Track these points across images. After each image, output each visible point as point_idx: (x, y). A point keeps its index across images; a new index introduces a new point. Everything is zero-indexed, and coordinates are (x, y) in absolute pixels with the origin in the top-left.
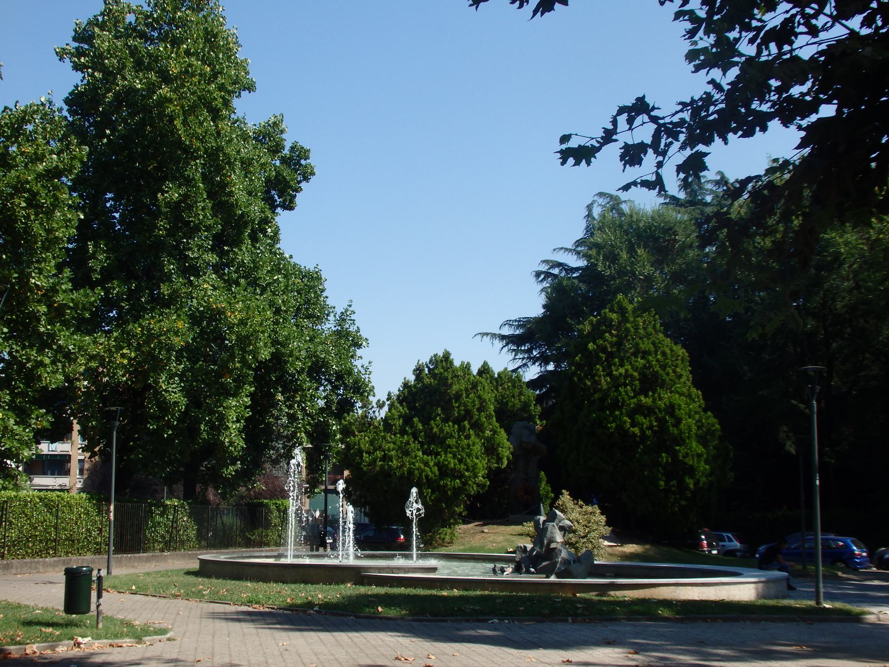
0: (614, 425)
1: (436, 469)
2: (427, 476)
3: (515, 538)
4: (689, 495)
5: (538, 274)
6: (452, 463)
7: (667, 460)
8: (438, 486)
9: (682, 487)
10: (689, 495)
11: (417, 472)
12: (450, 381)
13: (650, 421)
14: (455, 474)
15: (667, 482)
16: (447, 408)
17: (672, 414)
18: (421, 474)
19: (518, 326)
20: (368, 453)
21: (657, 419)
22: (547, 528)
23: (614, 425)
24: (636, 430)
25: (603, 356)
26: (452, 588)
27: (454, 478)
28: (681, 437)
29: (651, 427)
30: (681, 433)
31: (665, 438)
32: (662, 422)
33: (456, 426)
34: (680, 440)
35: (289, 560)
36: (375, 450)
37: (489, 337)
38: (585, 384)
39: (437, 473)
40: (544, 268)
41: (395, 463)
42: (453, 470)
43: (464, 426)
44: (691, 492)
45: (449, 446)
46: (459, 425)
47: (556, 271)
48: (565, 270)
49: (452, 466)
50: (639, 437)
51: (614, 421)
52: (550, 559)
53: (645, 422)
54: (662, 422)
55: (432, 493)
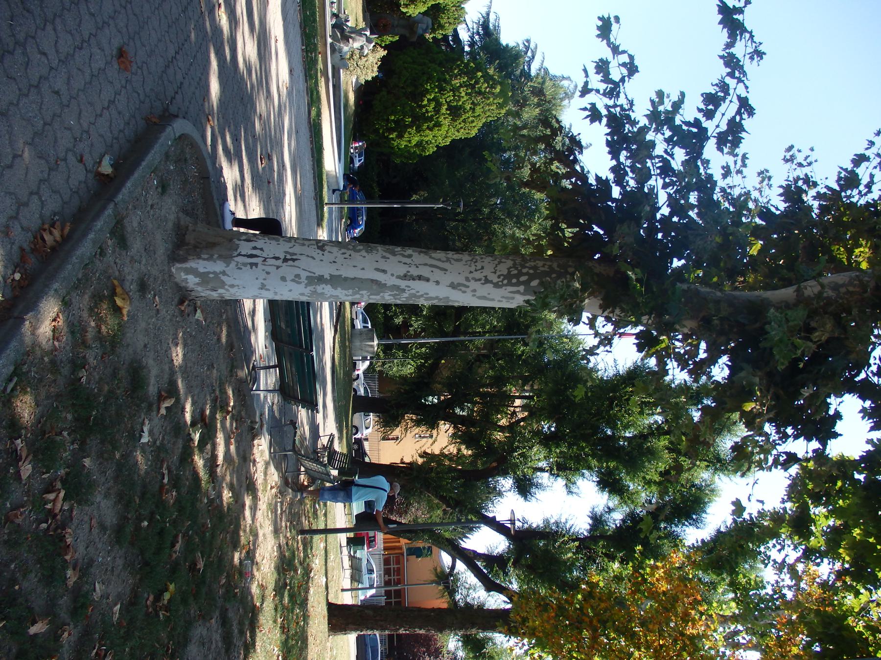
3: (354, 16)
5: (528, 41)
24: (425, 102)
25: (473, 82)
29: (427, 112)
32: (430, 119)
40: (532, 46)
47: (529, 54)
53: (430, 109)
54: (430, 119)
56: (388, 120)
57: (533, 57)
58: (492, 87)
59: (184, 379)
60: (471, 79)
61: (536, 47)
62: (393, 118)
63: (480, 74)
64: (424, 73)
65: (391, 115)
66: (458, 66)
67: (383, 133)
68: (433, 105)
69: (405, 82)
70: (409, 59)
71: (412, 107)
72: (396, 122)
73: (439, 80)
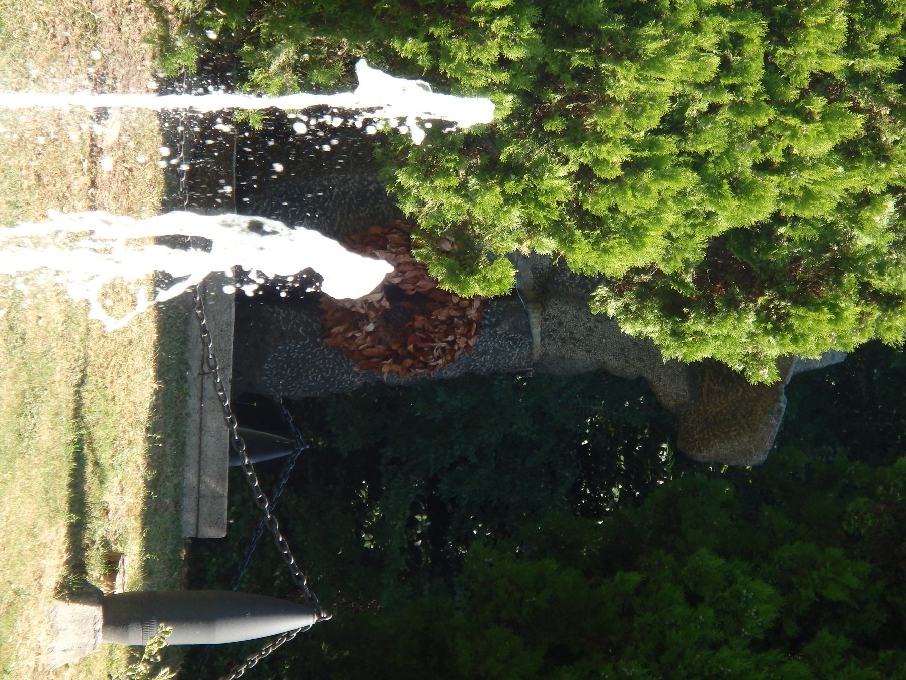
49: (624, 82)
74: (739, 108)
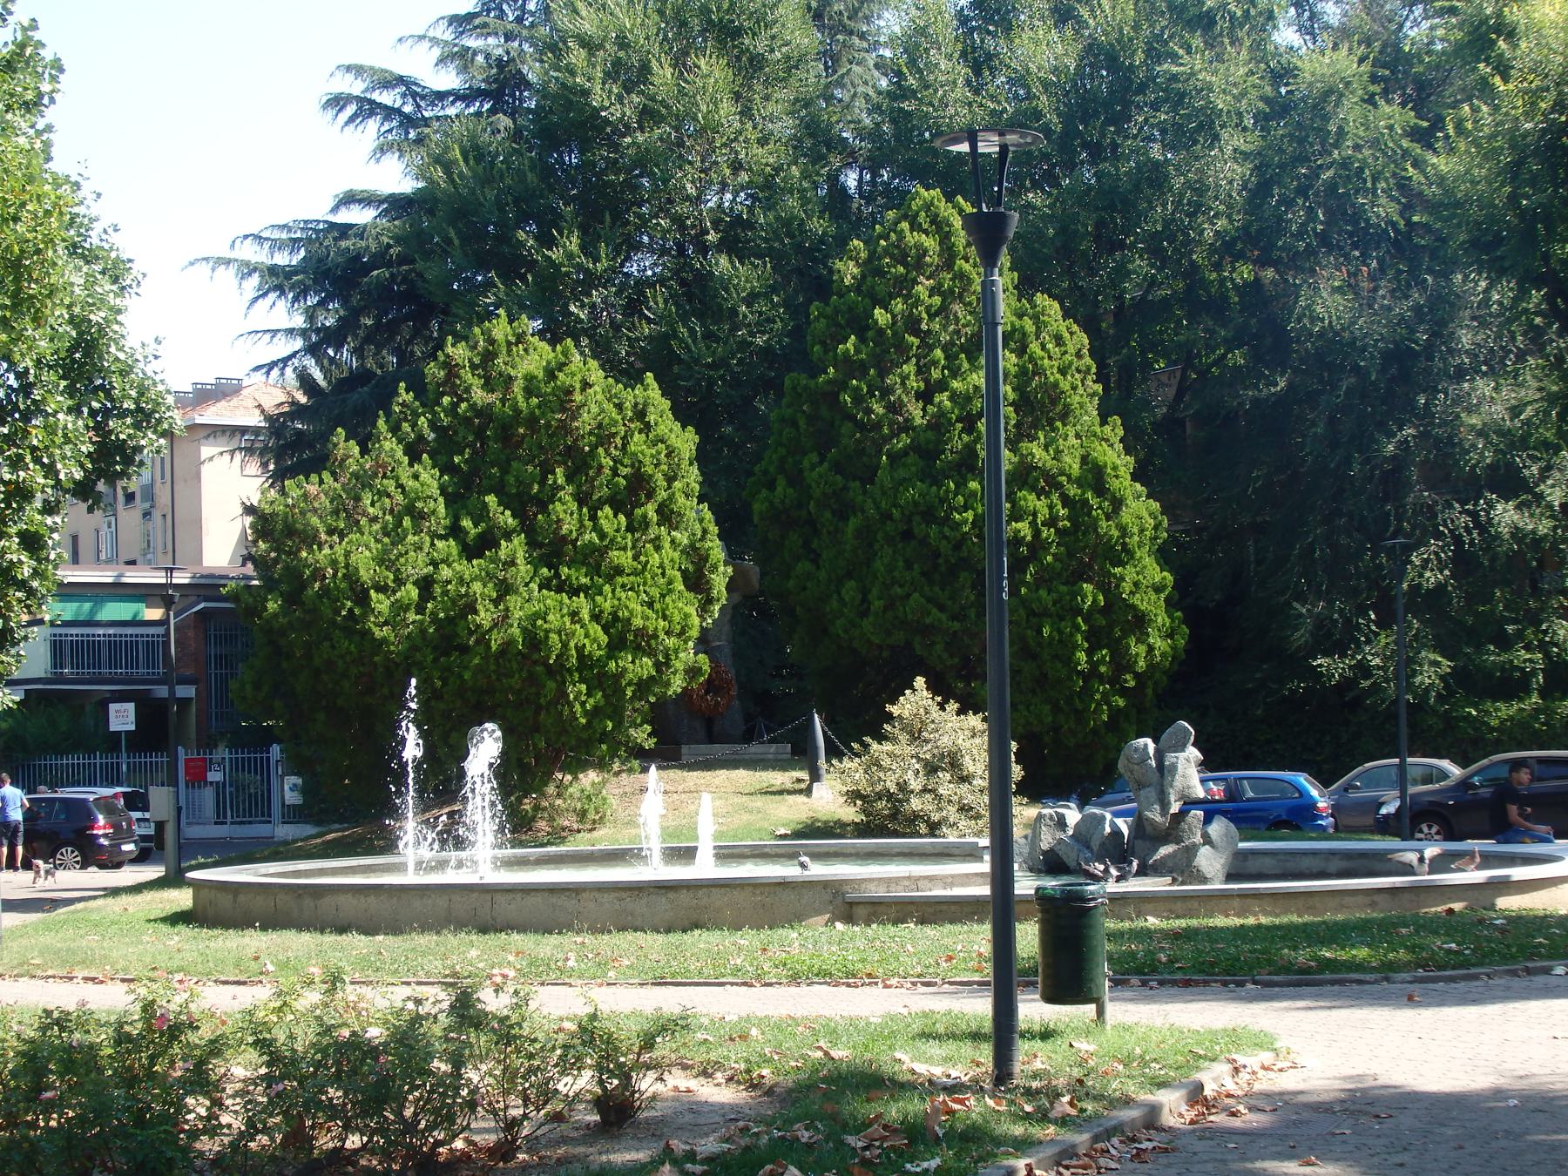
0: (970, 515)
1: (596, 630)
2: (580, 649)
3: (759, 802)
4: (1132, 684)
5: (337, 102)
6: (638, 614)
7: (1094, 601)
8: (603, 675)
9: (1122, 663)
10: (1132, 684)
11: (554, 637)
12: (578, 397)
13: (1051, 507)
14: (642, 643)
15: (1090, 653)
16: (580, 465)
17: (1101, 489)
18: (565, 645)
19: (277, 245)
20: (382, 589)
21: (1066, 501)
22: (1174, 767)
23: (970, 515)
24: (1024, 528)
25: (913, 340)
26: (1140, 914)
27: (638, 650)
28: (1124, 544)
29: (1052, 521)
30: (1123, 529)
31: (1088, 550)
32: (1077, 507)
33: (622, 518)
34: (1120, 554)
35: (411, 878)
36: (400, 582)
37: (232, 269)
38: (869, 411)
39: (604, 639)
40: (357, 87)
41: (484, 617)
42: (640, 632)
43: (645, 516)
44: (1137, 676)
45: (619, 571)
46: (629, 515)
47: (387, 98)
48: (414, 95)
49: (638, 622)
50: (1029, 545)
51: (966, 508)
52: (1178, 840)
53: (1040, 505)
54: (1077, 507)
55: (589, 695)
56: (1092, 674)
57: (401, 80)
58: (916, 262)
59: (24, 845)
60: (903, 349)
61: (357, 70)
62: (1082, 656)
63: (881, 316)
64: (907, 535)
65: (1070, 661)
66: (858, 399)
67: (1124, 692)
68: (1030, 500)
69: (942, 608)
70: (850, 589)
71: (1039, 581)
72: (1096, 640)
73: (934, 478)
74: (645, 584)
